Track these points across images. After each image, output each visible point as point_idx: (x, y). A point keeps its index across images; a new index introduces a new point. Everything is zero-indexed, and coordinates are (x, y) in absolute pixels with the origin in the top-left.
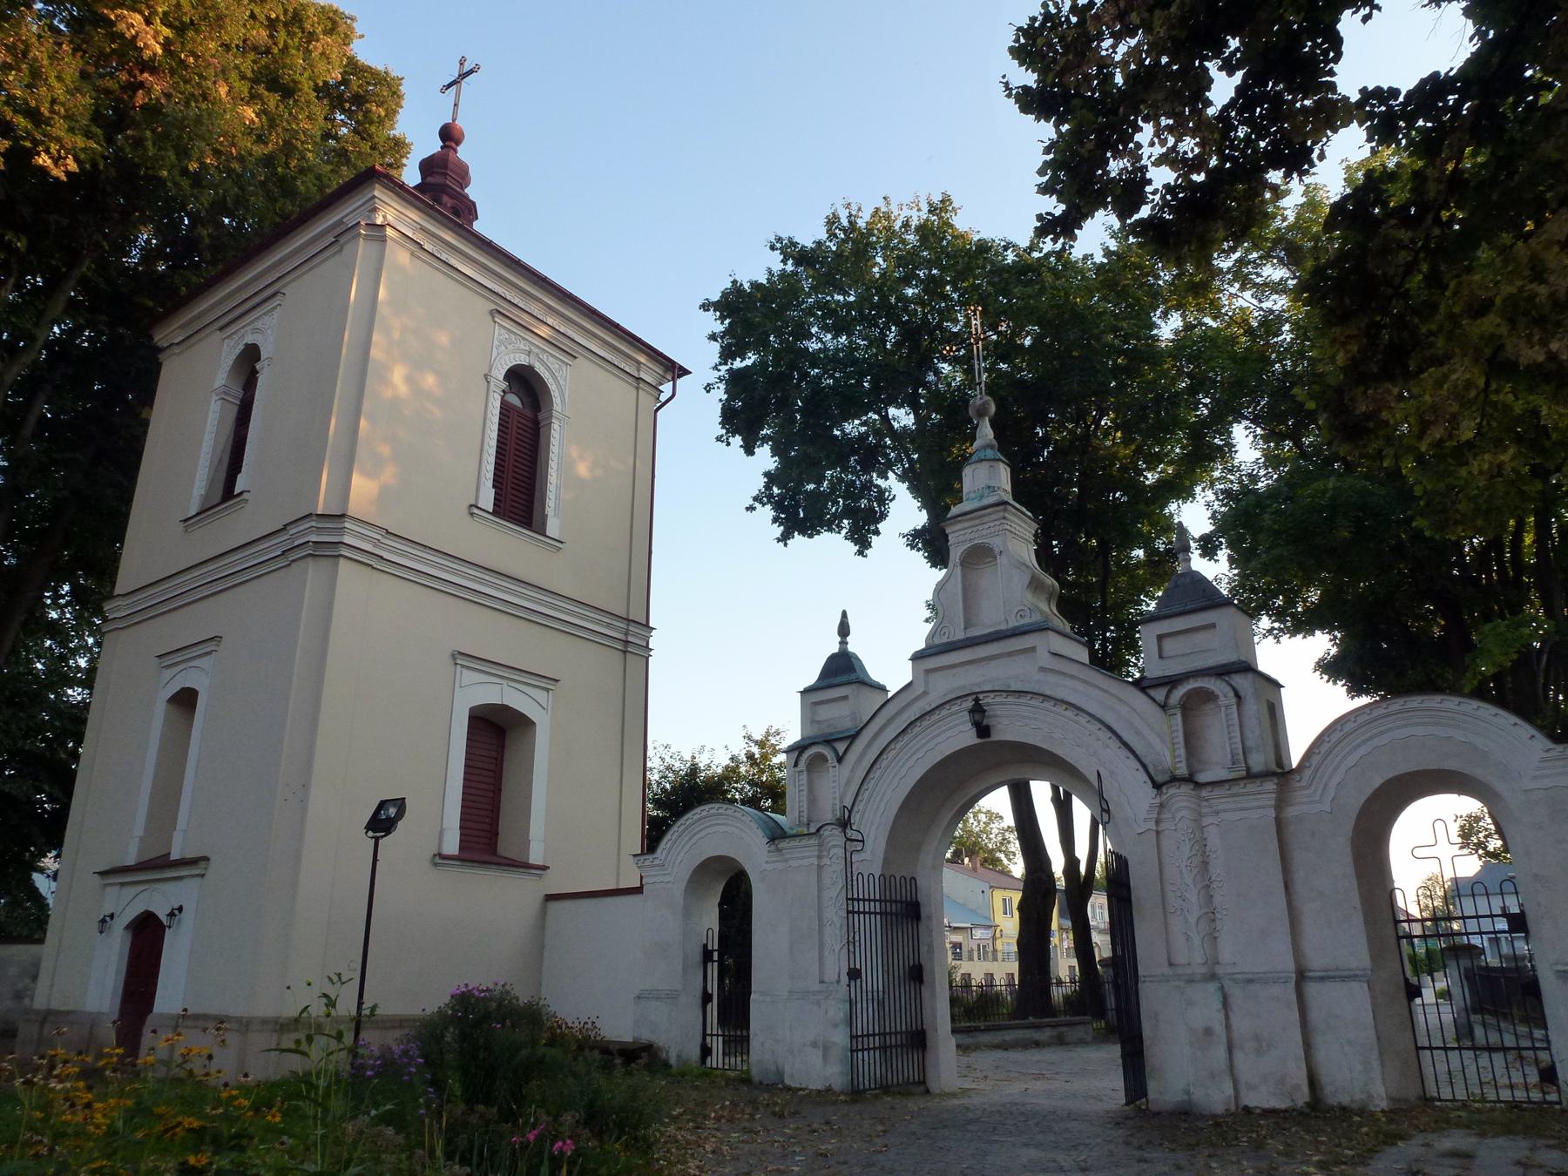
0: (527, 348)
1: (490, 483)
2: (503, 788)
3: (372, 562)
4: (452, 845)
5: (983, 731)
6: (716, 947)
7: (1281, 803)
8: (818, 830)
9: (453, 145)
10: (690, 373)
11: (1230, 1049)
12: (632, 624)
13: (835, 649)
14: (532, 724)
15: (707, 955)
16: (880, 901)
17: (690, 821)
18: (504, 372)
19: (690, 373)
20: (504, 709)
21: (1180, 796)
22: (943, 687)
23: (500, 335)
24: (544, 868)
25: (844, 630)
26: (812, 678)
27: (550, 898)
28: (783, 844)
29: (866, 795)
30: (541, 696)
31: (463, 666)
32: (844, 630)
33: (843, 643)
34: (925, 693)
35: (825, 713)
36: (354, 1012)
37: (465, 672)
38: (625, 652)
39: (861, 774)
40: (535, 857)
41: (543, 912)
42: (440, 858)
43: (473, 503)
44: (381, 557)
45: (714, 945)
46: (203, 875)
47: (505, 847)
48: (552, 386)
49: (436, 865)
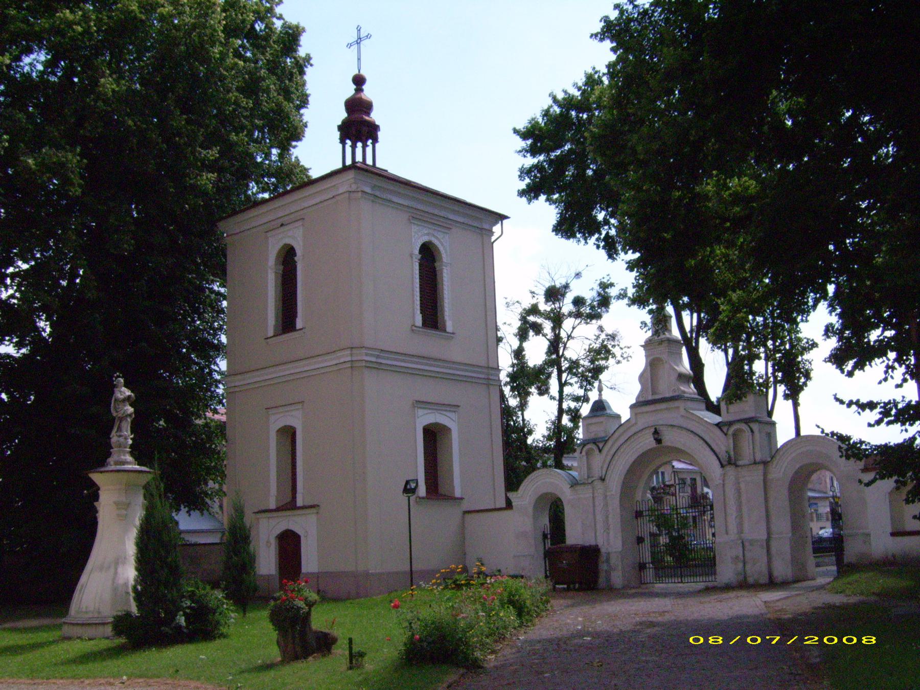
1: (419, 312)
5: (659, 441)
6: (549, 533)
7: (765, 474)
8: (592, 482)
11: (744, 564)
14: (449, 429)
15: (545, 536)
20: (437, 425)
21: (730, 470)
22: (643, 422)
24: (462, 499)
27: (466, 512)
28: (578, 488)
29: (610, 472)
30: (452, 415)
34: (636, 423)
35: (593, 428)
36: (408, 568)
37: (419, 410)
39: (609, 458)
41: (463, 517)
45: (548, 531)
47: (442, 490)
48: (441, 248)
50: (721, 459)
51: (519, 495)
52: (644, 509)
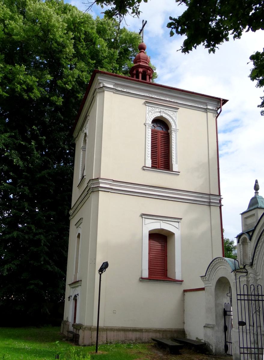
0: (160, 111)
2: (168, 255)
3: (107, 190)
4: (146, 274)
9: (143, 50)
10: (227, 101)
12: (211, 195)
13: (253, 195)
16: (248, 295)
17: (214, 264)
18: (151, 121)
19: (227, 101)
23: (149, 109)
24: (182, 281)
25: (256, 188)
26: (245, 208)
27: (185, 291)
30: (176, 224)
31: (145, 218)
32: (256, 188)
33: (257, 193)
37: (146, 219)
38: (210, 206)
40: (178, 277)
42: (142, 279)
43: (144, 166)
44: (112, 189)
46: (81, 285)
47: (169, 275)
49: (141, 281)
50: (251, 341)
51: (207, 279)
52: (227, 310)
